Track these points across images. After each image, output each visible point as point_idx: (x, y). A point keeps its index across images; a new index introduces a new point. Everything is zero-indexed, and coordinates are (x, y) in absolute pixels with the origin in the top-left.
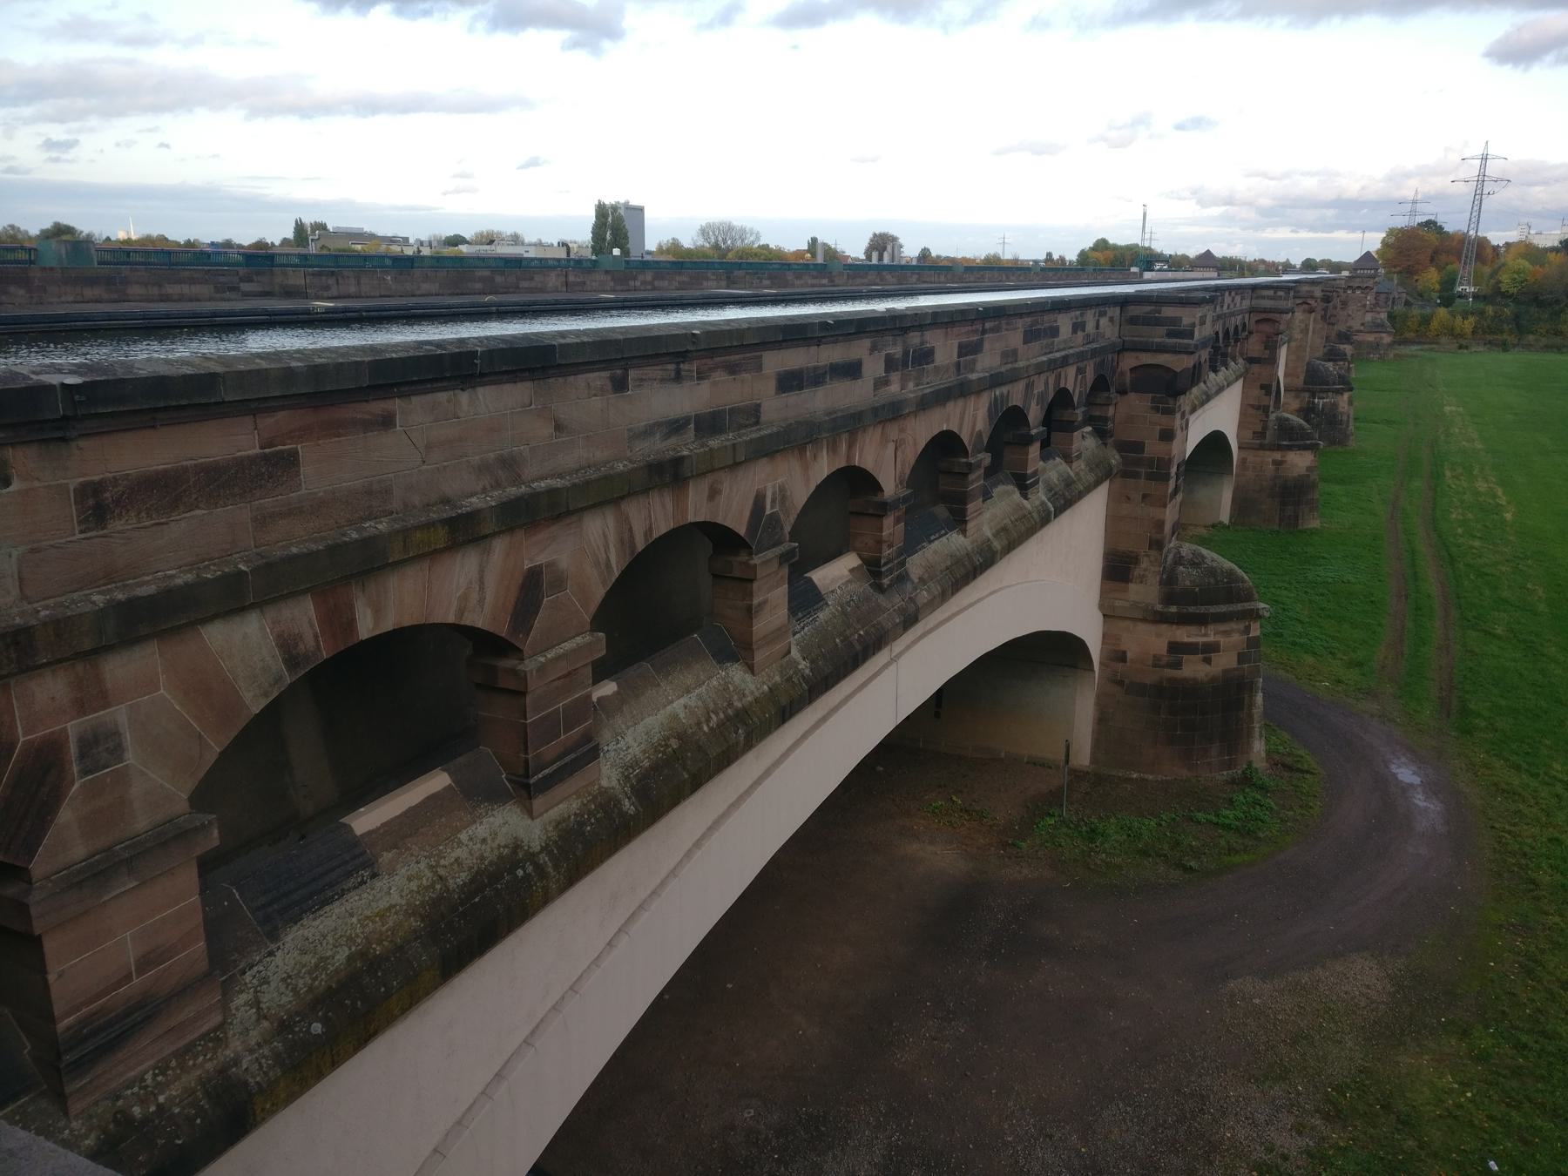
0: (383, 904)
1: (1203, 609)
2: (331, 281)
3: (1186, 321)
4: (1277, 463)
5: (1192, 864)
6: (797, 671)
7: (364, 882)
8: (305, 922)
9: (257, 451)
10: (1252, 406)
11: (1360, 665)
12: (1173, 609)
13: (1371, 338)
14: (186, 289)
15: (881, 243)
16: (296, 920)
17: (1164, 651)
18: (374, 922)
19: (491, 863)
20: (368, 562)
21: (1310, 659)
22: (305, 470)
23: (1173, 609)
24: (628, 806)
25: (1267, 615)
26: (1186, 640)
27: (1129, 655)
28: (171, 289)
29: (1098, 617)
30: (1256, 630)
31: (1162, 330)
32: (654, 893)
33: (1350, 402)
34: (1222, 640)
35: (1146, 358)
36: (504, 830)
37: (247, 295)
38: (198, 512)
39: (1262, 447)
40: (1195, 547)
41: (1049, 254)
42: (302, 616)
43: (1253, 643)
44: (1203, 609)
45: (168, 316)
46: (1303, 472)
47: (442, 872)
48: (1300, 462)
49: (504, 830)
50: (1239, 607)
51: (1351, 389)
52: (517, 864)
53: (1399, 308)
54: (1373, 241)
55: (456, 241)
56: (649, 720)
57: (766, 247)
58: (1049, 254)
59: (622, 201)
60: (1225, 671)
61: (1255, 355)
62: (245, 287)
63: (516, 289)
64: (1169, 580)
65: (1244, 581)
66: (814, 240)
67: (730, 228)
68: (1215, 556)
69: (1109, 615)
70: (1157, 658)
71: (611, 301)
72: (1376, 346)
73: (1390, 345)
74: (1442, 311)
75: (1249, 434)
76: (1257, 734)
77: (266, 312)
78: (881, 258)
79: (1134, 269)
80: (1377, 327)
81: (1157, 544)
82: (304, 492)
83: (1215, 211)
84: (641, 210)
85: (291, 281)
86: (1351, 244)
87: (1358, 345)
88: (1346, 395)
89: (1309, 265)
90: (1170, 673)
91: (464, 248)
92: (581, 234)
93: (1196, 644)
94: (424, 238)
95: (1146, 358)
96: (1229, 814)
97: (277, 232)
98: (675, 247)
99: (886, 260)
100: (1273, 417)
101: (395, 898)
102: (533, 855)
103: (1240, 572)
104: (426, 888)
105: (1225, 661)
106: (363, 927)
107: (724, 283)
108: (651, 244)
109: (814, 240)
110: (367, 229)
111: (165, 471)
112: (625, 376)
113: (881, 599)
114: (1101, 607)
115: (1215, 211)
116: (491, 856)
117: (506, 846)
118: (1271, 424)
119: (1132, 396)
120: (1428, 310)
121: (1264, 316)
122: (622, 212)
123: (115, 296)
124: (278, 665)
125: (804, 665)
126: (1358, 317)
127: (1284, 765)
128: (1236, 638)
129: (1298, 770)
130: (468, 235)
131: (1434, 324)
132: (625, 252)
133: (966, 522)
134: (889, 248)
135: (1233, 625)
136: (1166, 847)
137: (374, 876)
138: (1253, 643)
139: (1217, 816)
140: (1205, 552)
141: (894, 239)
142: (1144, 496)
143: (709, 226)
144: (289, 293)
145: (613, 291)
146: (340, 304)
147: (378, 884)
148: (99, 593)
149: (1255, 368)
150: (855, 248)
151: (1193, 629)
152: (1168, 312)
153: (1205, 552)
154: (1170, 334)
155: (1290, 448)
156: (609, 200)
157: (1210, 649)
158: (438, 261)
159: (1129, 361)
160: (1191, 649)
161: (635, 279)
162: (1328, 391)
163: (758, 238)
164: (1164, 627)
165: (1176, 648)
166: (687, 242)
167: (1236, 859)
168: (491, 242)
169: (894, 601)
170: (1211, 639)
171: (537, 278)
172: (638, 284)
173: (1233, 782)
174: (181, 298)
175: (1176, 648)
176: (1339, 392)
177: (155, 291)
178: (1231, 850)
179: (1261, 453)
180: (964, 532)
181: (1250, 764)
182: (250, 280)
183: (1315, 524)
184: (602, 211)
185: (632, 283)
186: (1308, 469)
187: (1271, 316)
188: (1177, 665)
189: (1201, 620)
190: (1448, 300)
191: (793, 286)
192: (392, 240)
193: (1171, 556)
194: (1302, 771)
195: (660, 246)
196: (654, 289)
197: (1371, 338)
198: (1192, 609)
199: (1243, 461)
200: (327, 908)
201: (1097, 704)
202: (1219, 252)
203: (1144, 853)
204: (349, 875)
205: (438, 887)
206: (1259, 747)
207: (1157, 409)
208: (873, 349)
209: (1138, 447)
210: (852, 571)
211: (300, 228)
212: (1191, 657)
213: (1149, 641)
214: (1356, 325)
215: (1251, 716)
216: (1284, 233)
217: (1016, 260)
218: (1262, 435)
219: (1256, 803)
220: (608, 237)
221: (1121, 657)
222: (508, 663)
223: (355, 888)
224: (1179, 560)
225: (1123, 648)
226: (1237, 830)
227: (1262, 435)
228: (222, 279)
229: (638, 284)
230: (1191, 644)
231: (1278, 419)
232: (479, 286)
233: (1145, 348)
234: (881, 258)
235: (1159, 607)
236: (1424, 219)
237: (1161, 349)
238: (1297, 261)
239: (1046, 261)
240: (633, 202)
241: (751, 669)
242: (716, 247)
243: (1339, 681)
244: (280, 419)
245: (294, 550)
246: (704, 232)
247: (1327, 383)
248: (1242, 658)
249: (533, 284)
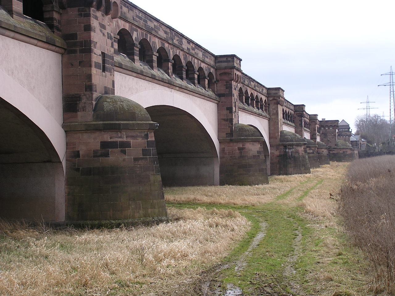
10: (224, 120)
17: (98, 147)
27: (81, 153)
29: (62, 132)
34: (132, 141)
39: (231, 141)
61: (222, 92)
70: (95, 152)
75: (224, 135)
93: (116, 142)
114: (63, 127)
121: (222, 71)
128: (140, 140)
149: (223, 99)
157: (124, 146)
160: (113, 145)
164: (97, 134)
175: (105, 145)
179: (231, 144)
186: (258, 152)
187: (226, 71)
188: (107, 155)
199: (222, 150)
209: (73, 36)
212: (115, 150)
221: (77, 154)
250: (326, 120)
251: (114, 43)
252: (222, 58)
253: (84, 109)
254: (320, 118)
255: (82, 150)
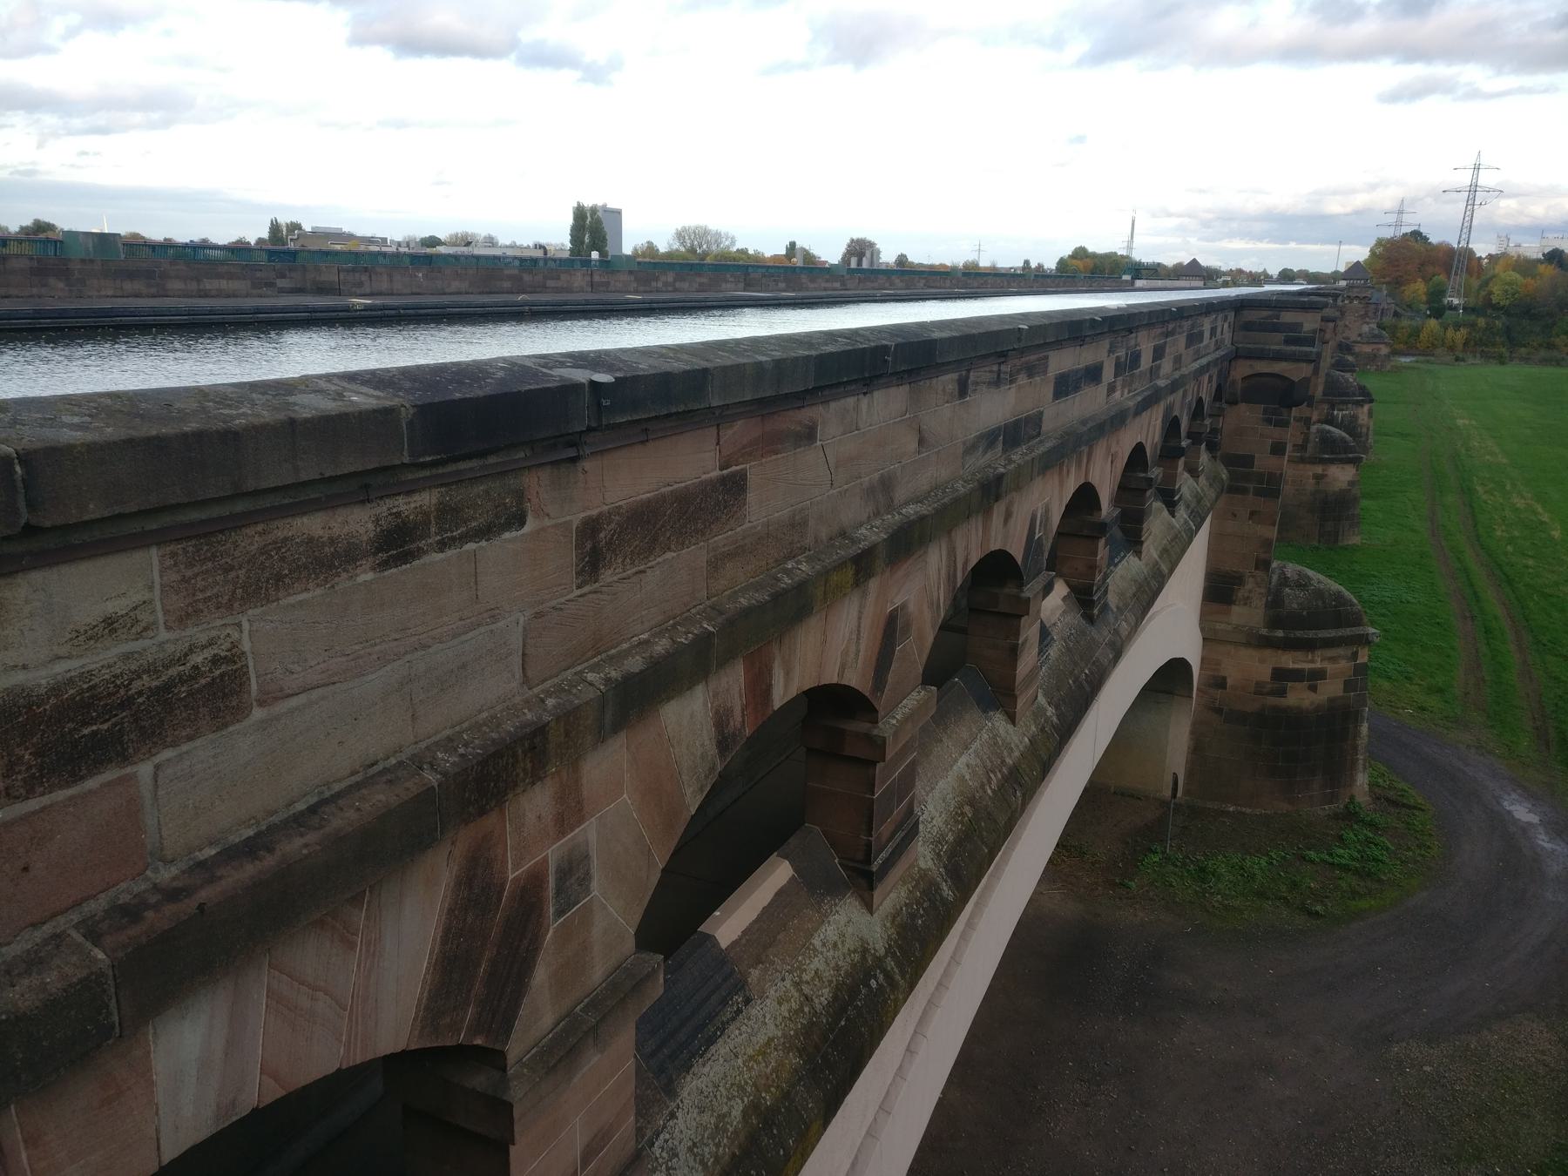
0: (761, 1039)
1: (1311, 634)
2: (364, 278)
3: (1307, 327)
4: (1319, 478)
5: (1319, 908)
6: (1047, 719)
7: (739, 1011)
8: (695, 1069)
9: (716, 473)
11: (1440, 691)
12: (1280, 633)
13: (1368, 349)
14: (224, 284)
15: (859, 249)
16: (687, 1067)
18: (758, 1063)
19: (847, 974)
20: (792, 607)
21: (1386, 685)
22: (751, 497)
23: (1280, 633)
24: (947, 891)
25: (1377, 640)
26: (1291, 666)
27: (1229, 682)
28: (208, 285)
30: (1363, 658)
31: (1281, 336)
32: (940, 984)
33: (1370, 414)
34: (1328, 666)
35: (1262, 367)
36: (850, 930)
37: (282, 291)
38: (669, 555)
39: (1302, 460)
40: (1299, 568)
41: (1027, 262)
42: (733, 681)
43: (1361, 670)
44: (1311, 634)
45: (211, 312)
46: (1344, 486)
47: (806, 989)
48: (1341, 475)
49: (850, 930)
50: (1348, 632)
51: (1371, 401)
52: (868, 975)
53: (1388, 320)
54: (1360, 253)
55: (433, 242)
56: (941, 784)
57: (744, 252)
58: (1027, 262)
59: (600, 203)
60: (1331, 700)
62: (281, 283)
63: (543, 288)
64: (1275, 602)
65: (1352, 605)
66: (793, 245)
67: (706, 232)
68: (1321, 577)
69: (1210, 639)
71: (638, 302)
72: (1373, 357)
73: (1388, 356)
74: (1433, 322)
76: (1361, 767)
77: (307, 309)
78: (860, 263)
79: (1126, 277)
80: (1374, 339)
81: (1264, 565)
82: (747, 525)
83: (1174, 222)
84: (619, 212)
85: (323, 278)
86: (1332, 257)
87: (1357, 355)
88: (1366, 407)
89: (1287, 276)
90: (1272, 701)
91: (442, 249)
92: (557, 234)
93: (1302, 670)
94: (400, 239)
95: (1262, 367)
96: (1343, 854)
97: (255, 232)
98: (651, 249)
99: (865, 265)
100: (1314, 428)
101: (772, 1030)
102: (879, 961)
103: (1346, 593)
104: (796, 1012)
105: (1331, 689)
106: (750, 1069)
107: (741, 285)
108: (627, 249)
109: (793, 245)
110: (346, 229)
111: (649, 501)
112: (967, 377)
113: (1093, 631)
115: (1174, 222)
116: (845, 965)
117: (855, 951)
118: (1312, 437)
119: (1243, 407)
120: (1417, 322)
122: (600, 214)
123: (153, 290)
124: (712, 750)
125: (1050, 711)
126: (1357, 328)
127: (1387, 800)
128: (1343, 664)
129: (1404, 805)
130: (442, 236)
131: (1423, 336)
132: (603, 254)
133: (1142, 543)
134: (868, 254)
135: (1341, 651)
136: (1283, 888)
137: (748, 1001)
138: (1361, 670)
139: (1331, 855)
140: (1310, 573)
141: (871, 245)
142: (1252, 514)
143: (684, 230)
144: (321, 290)
145: (636, 292)
146: (378, 301)
147: (754, 1011)
148: (592, 669)
150: (831, 253)
151: (1299, 655)
152: (1288, 317)
153: (1310, 573)
154: (1288, 342)
155: (1332, 461)
156: (588, 203)
157: (1319, 675)
158: (416, 259)
159: (1242, 370)
160: (1296, 675)
161: (657, 279)
162: (1346, 403)
163: (733, 243)
164: (1268, 652)
165: (1281, 675)
166: (663, 248)
167: (1363, 904)
168: (468, 244)
169: (1102, 635)
170: (1318, 665)
171: (563, 277)
172: (660, 285)
173: (1335, 817)
174: (220, 294)
175: (1281, 675)
176: (1359, 404)
177: (193, 286)
178: (1355, 894)
180: (1138, 554)
181: (1352, 798)
182: (283, 276)
183: (1355, 540)
184: (580, 214)
185: (654, 284)
186: (1351, 483)
188: (1282, 693)
189: (1309, 646)
190: (1438, 312)
191: (807, 289)
192: (370, 240)
193: (1275, 578)
194: (1409, 807)
195: (635, 249)
196: (676, 290)
197: (1368, 349)
198: (1299, 634)
200: (713, 1049)
201: (1192, 733)
202: (1204, 261)
203: (1261, 895)
204: (724, 1002)
205: (806, 1009)
206: (1362, 780)
207: (1269, 421)
208: (1110, 351)
209: (1248, 461)
210: (1064, 599)
211: (275, 228)
213: (1251, 667)
214: (1354, 337)
215: (1355, 748)
216: (1238, 245)
217: (994, 268)
218: (1303, 447)
219: (1368, 841)
220: (587, 239)
221: (1221, 683)
222: (860, 726)
223: (733, 1019)
224: (1284, 581)
225: (1222, 674)
226: (1356, 872)
227: (1303, 447)
228: (258, 274)
229: (660, 285)
230: (1298, 671)
231: (1318, 431)
232: (507, 285)
233: (1260, 355)
234: (860, 263)
235: (1264, 631)
236: (1409, 230)
237: (1279, 357)
238: (1274, 271)
239: (1024, 268)
240: (612, 205)
241: (1012, 719)
242: (692, 250)
243: (1423, 709)
244: (739, 431)
245: (744, 601)
246: (680, 235)
247: (1347, 394)
248: (1349, 685)
249: (559, 284)
250: (631, 239)
251: (1318, 317)
252: (280, 523)
253: (1246, 601)
254: (631, 239)
255: (1232, 674)
